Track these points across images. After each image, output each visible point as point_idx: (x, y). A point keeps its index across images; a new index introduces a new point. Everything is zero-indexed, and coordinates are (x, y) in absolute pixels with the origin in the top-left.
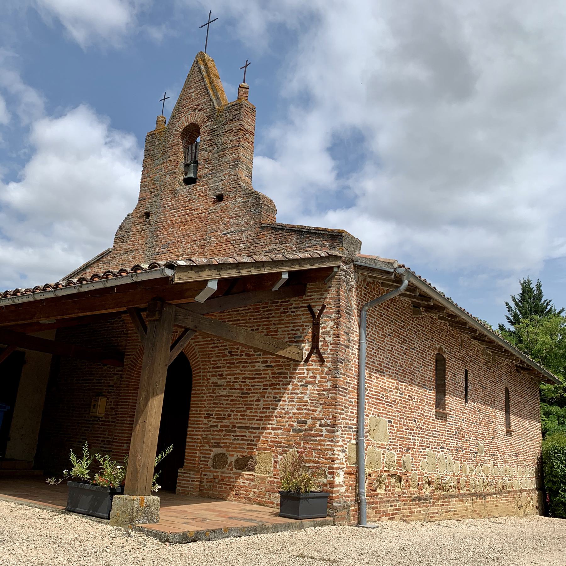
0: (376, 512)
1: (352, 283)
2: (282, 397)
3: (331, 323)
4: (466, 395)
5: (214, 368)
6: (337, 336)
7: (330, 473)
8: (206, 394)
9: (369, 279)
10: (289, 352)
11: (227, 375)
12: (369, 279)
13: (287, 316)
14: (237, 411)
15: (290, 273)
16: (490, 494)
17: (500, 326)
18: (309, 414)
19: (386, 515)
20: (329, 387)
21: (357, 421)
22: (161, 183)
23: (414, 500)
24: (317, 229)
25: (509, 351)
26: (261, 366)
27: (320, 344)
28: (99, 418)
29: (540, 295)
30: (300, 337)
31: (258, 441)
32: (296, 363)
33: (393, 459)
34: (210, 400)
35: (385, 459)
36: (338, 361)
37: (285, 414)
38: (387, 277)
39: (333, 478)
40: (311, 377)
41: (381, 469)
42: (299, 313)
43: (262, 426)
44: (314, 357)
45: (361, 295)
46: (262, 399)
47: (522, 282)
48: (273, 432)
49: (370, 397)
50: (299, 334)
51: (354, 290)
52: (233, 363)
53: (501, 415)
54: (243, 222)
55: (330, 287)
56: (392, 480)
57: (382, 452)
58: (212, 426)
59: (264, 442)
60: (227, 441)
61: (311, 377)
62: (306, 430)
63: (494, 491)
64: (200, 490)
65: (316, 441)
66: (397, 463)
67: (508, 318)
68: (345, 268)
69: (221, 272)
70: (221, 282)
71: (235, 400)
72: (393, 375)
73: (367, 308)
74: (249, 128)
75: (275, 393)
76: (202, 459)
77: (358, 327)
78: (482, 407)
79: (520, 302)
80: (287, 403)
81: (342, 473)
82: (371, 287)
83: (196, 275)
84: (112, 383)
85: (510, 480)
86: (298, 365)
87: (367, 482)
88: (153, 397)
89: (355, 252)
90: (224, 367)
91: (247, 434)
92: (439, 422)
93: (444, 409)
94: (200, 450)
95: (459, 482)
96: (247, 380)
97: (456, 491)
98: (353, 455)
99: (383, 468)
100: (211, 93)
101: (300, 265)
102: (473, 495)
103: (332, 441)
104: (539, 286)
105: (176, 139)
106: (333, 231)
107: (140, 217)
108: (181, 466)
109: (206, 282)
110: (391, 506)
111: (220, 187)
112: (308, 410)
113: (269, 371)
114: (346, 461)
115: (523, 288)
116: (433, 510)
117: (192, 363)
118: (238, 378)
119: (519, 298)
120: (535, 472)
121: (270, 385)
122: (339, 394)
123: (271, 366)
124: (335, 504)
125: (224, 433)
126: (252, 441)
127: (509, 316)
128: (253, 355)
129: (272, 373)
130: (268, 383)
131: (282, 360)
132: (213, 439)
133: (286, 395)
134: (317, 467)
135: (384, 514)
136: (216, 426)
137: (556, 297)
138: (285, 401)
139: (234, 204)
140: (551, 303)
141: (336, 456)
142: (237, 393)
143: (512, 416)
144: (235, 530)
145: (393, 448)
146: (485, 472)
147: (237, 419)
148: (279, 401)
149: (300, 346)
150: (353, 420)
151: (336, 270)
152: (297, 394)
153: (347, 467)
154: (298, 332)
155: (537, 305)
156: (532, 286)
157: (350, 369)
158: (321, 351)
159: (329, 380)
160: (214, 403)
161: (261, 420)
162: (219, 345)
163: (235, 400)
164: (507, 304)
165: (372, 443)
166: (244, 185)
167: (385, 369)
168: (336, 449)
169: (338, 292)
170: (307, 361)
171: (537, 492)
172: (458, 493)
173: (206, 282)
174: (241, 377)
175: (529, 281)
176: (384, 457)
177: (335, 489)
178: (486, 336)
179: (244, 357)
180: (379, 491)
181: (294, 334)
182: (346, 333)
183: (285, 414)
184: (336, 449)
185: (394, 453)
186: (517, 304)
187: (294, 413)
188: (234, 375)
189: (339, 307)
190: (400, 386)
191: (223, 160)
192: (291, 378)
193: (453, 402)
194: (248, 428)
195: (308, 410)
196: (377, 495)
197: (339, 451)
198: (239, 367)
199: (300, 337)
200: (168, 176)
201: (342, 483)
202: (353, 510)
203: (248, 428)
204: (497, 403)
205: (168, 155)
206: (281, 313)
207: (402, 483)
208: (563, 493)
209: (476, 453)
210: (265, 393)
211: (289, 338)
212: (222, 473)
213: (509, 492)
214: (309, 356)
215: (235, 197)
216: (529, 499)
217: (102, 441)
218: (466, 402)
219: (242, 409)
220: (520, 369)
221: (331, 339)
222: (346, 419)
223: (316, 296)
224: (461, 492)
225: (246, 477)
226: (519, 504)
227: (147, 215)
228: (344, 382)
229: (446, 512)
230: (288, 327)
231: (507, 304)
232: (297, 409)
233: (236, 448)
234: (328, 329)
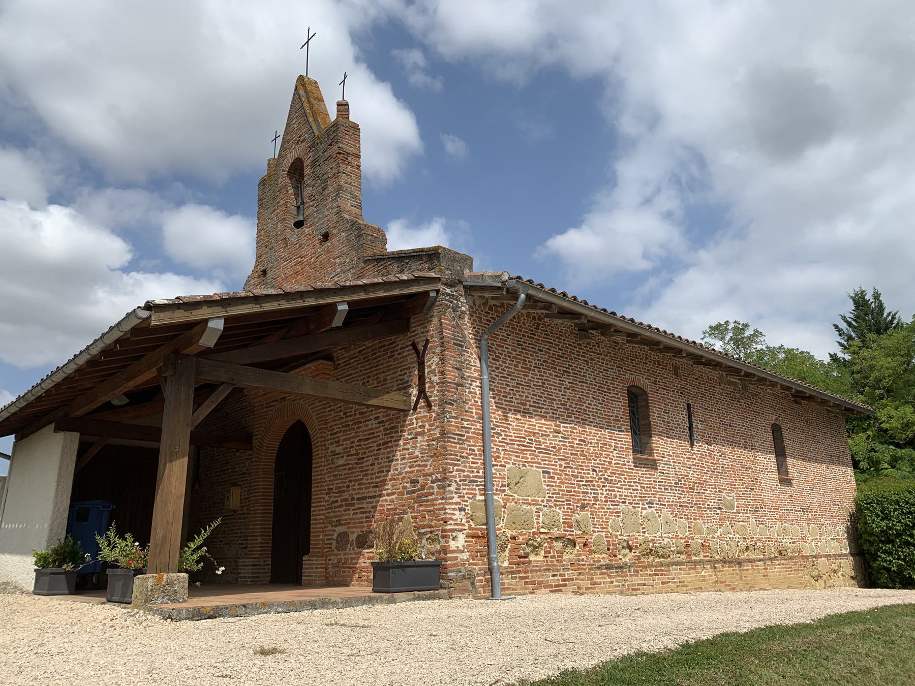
0: (526, 583)
1: (464, 309)
2: (394, 456)
3: (436, 359)
4: (691, 436)
5: (331, 435)
6: (442, 373)
7: (443, 537)
8: (325, 466)
9: (492, 302)
10: (390, 400)
11: (344, 440)
12: (492, 302)
13: (394, 360)
14: (355, 481)
15: (349, 303)
16: (751, 561)
17: (831, 356)
18: (420, 471)
19: (545, 587)
20: (438, 435)
21: (484, 473)
22: (274, 233)
23: (599, 568)
24: (414, 251)
25: (754, 375)
26: (373, 424)
27: (427, 386)
28: (235, 511)
29: (881, 307)
30: (407, 382)
31: (375, 512)
32: (405, 412)
33: (557, 517)
34: (330, 473)
35: (541, 519)
36: (446, 403)
37: (398, 474)
38: (497, 294)
39: (447, 542)
40: (420, 427)
41: (535, 530)
42: (406, 353)
43: (378, 493)
44: (422, 403)
45: (481, 322)
46: (376, 462)
47: (852, 295)
48: (388, 498)
49: (508, 444)
50: (406, 379)
51: (467, 317)
52: (348, 426)
53: (770, 460)
54: (348, 260)
55: (432, 317)
56: (558, 545)
57: (535, 510)
58: (333, 502)
59: (382, 512)
60: (348, 517)
61: (420, 427)
62: (418, 490)
63: (762, 557)
64: (327, 578)
65: (428, 501)
66: (564, 523)
67: (841, 344)
68: (448, 291)
69: (228, 309)
70: (227, 320)
71: (353, 468)
72: (548, 416)
73: (486, 336)
74: (351, 150)
75: (389, 453)
76: (326, 542)
77: (478, 361)
78: (727, 450)
79: (855, 320)
80: (399, 462)
81: (461, 537)
82: (498, 312)
83: (188, 313)
84: (244, 470)
85: (794, 543)
86: (407, 416)
87: (509, 547)
88: (171, 461)
89: (462, 271)
90: (340, 432)
91: (365, 506)
92: (641, 471)
93: (651, 454)
94: (323, 532)
95: (687, 546)
96: (362, 443)
97: (683, 557)
98: (481, 514)
99: (538, 529)
100: (311, 120)
101: (366, 292)
102: (717, 561)
103: (443, 498)
104: (877, 296)
105: (284, 179)
106: (429, 249)
107: (259, 277)
108: (307, 552)
109: (207, 320)
110: (554, 576)
111: (325, 225)
112: (419, 465)
113: (381, 428)
114: (468, 522)
115: (856, 303)
116: (636, 580)
117: (311, 432)
118: (353, 442)
119: (852, 316)
120: (847, 532)
121: (383, 444)
122: (449, 441)
123: (383, 422)
124: (450, 574)
125: (344, 507)
126: (370, 512)
127: (842, 341)
128: (366, 412)
129: (386, 430)
130: (381, 442)
131: (393, 412)
132: (336, 516)
133: (398, 453)
134: (431, 532)
135: (540, 585)
136: (337, 501)
137: (905, 306)
138: (397, 460)
139: (339, 239)
140: (897, 316)
141: (448, 516)
142: (353, 460)
143: (790, 461)
144: (279, 605)
145: (556, 505)
146: (741, 533)
147: (354, 490)
148: (392, 461)
149: (407, 393)
150: (478, 472)
151: (433, 294)
152: (408, 449)
153: (470, 528)
154: (405, 377)
155: (877, 322)
156: (867, 298)
157: (466, 411)
158: (428, 394)
159: (437, 427)
160: (334, 476)
161: (377, 487)
162: (335, 407)
163: (353, 468)
164: (836, 326)
165: (513, 499)
166: (348, 217)
167: (531, 409)
168: (447, 507)
169: (440, 321)
170: (415, 409)
171: (851, 558)
172: (687, 560)
173: (207, 320)
174: (356, 440)
175: (863, 292)
176: (539, 516)
177: (449, 555)
178: (702, 357)
179: (358, 416)
180: (532, 558)
181: (401, 380)
182: (457, 369)
183: (398, 474)
184: (447, 507)
185: (557, 510)
186: (849, 324)
187: (407, 473)
188: (349, 439)
189: (442, 338)
190: (562, 429)
191: (326, 192)
192: (402, 431)
193: (661, 445)
194: (364, 498)
195: (419, 465)
196: (530, 562)
197: (454, 509)
198: (354, 429)
199: (407, 382)
200: (280, 224)
201: (462, 548)
202: (481, 581)
203: (364, 498)
204: (757, 445)
205: (278, 199)
206: (389, 357)
207: (577, 547)
208: (883, 556)
209: (720, 508)
210: (379, 454)
211: (398, 385)
212: (345, 554)
213: (791, 558)
214: (417, 402)
215: (340, 232)
216: (834, 567)
217: (240, 537)
218: (692, 445)
219: (359, 477)
220: (798, 400)
221: (436, 378)
222: (464, 471)
223: (420, 330)
224: (694, 558)
225: (366, 555)
226: (815, 573)
227: (264, 272)
228: (457, 427)
229: (663, 583)
230: (395, 373)
231: (836, 326)
232: (410, 467)
233: (355, 523)
234: (433, 367)
